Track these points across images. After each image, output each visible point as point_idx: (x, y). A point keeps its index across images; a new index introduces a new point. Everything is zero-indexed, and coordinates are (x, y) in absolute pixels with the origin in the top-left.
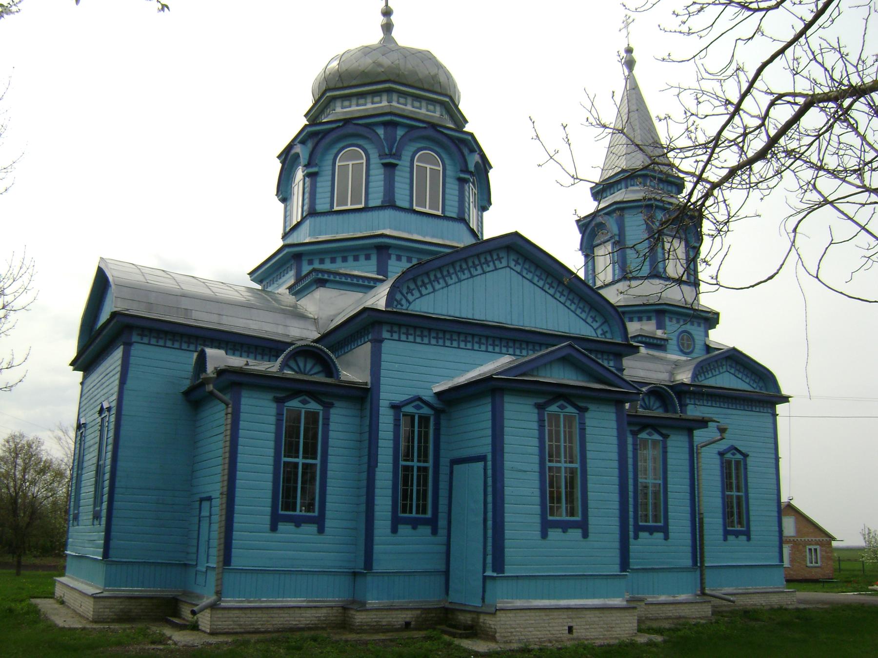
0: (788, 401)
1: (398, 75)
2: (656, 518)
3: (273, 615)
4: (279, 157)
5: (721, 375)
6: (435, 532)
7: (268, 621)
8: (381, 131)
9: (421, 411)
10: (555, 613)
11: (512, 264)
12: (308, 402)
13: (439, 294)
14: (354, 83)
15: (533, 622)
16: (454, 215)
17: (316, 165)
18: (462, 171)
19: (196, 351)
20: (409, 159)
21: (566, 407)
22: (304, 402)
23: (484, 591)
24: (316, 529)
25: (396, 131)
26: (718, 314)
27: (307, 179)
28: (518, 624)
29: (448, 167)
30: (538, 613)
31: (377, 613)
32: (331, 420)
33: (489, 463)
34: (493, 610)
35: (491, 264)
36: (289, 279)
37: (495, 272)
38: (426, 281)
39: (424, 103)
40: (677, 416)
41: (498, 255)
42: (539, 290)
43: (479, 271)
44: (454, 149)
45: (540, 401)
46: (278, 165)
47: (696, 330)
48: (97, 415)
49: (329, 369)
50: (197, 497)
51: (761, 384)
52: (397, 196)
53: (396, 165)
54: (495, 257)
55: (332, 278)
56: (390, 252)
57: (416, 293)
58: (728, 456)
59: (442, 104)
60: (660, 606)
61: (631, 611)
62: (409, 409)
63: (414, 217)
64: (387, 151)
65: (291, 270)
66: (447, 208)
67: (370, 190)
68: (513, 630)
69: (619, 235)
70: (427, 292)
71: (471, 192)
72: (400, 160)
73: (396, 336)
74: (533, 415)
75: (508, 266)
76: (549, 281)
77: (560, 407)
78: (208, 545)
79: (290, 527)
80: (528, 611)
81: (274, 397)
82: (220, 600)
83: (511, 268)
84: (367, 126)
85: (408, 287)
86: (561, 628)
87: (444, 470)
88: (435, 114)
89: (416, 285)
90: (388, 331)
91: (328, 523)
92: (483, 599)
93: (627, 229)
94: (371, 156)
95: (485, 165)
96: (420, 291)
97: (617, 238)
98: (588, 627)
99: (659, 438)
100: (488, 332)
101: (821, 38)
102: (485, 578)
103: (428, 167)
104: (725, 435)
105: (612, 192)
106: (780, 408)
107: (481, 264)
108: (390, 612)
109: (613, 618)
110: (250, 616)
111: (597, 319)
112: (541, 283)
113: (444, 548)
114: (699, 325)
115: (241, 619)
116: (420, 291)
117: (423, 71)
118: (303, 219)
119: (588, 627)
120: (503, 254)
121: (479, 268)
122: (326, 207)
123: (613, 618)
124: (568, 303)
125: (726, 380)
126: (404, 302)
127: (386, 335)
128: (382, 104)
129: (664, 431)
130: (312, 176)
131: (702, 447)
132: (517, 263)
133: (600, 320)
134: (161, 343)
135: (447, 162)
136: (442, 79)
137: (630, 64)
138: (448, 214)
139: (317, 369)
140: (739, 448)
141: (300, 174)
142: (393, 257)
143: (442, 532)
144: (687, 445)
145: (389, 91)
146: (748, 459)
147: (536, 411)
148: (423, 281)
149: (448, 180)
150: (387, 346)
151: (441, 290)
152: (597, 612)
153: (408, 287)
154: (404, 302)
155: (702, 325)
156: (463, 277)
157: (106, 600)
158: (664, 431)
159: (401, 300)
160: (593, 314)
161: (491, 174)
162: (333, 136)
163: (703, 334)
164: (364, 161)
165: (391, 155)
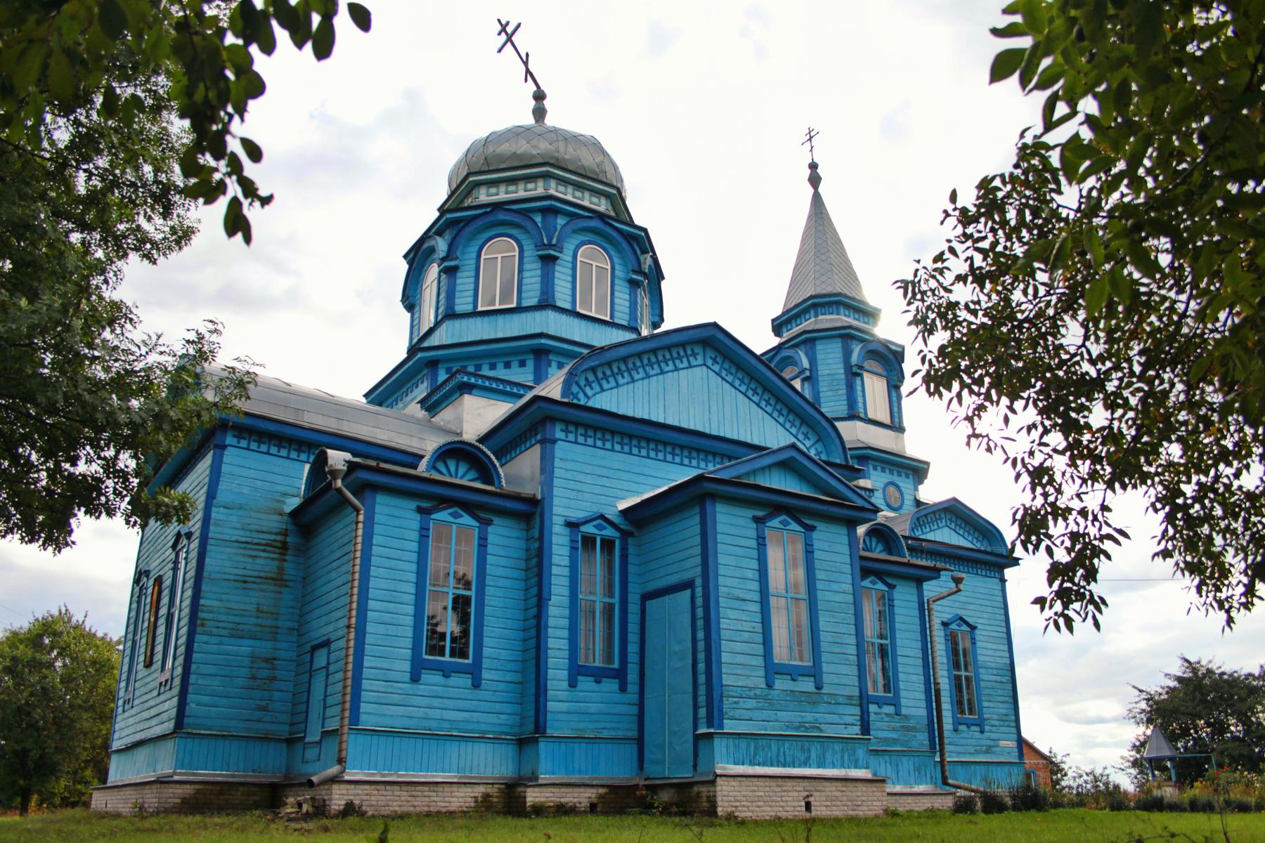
0: (1018, 564)
1: (557, 159)
2: (887, 688)
3: (414, 793)
4: (405, 257)
5: (940, 530)
6: (623, 688)
7: (408, 801)
8: (538, 219)
9: (604, 532)
10: (789, 784)
11: (709, 362)
12: (459, 516)
13: (623, 390)
14: (503, 166)
15: (762, 794)
16: (625, 323)
17: (456, 258)
18: (634, 272)
19: (307, 462)
20: (571, 253)
21: (790, 524)
22: (456, 516)
23: (696, 755)
24: (470, 682)
25: (375, 499)
26: (928, 464)
27: (444, 276)
28: (744, 796)
29: (617, 267)
30: (768, 782)
31: (553, 790)
32: (490, 540)
33: (699, 591)
34: (711, 778)
35: (685, 360)
36: (422, 390)
37: (690, 370)
38: (608, 373)
39: (587, 194)
40: (905, 560)
41: (692, 350)
42: (741, 396)
43: (671, 367)
44: (624, 245)
45: (760, 513)
46: (404, 267)
47: (905, 484)
48: (170, 550)
49: (487, 474)
50: (308, 647)
51: (985, 543)
52: (557, 295)
53: (556, 258)
54: (689, 352)
55: (480, 382)
56: (551, 357)
57: (596, 387)
58: (953, 626)
59: (607, 196)
60: (897, 797)
61: (879, 785)
62: (589, 529)
63: (576, 321)
64: (546, 242)
65: (422, 382)
66: (616, 314)
67: (524, 288)
68: (738, 804)
69: (810, 370)
70: (609, 386)
71: (644, 300)
72: (561, 252)
73: (571, 437)
74: (751, 530)
75: (705, 365)
76: (753, 386)
77: (784, 523)
78: (325, 704)
79: (436, 678)
80: (755, 780)
81: (418, 507)
82: (343, 771)
83: (708, 367)
84: (518, 212)
85: (586, 379)
86: (796, 804)
87: (633, 609)
88: (603, 206)
89: (597, 378)
90: (562, 430)
91: (486, 675)
92: (695, 766)
93: (819, 362)
94: (526, 248)
95: (657, 274)
96: (601, 386)
97: (808, 373)
98: (829, 803)
99: (884, 588)
100: (685, 439)
101: (815, 180)
102: (698, 738)
103: (594, 264)
104: (961, 586)
105: (798, 322)
106: (1008, 573)
107: (673, 359)
108: (571, 790)
109: (859, 794)
110: (384, 793)
111: (809, 436)
112: (743, 388)
113: (635, 710)
114: (907, 476)
115: (372, 798)
116: (601, 386)
117: (588, 160)
118: (438, 324)
119: (829, 803)
120: (698, 349)
121: (670, 363)
122: (469, 308)
123: (859, 794)
124: (775, 414)
125: (946, 535)
126: (581, 395)
127: (559, 434)
128: (539, 189)
129: (889, 581)
130: (450, 271)
131: (934, 601)
132: (715, 361)
133: (813, 438)
134: (264, 448)
135: (616, 260)
136: (608, 168)
137: (815, 180)
138: (616, 321)
139: (472, 474)
140: (966, 618)
141: (433, 271)
142: (554, 364)
143: (633, 688)
144: (915, 598)
145: (546, 176)
146: (977, 632)
147: (754, 526)
148: (604, 373)
149: (617, 281)
150: (561, 449)
151: (626, 387)
152: (838, 784)
153: (586, 379)
154: (581, 395)
155: (911, 477)
156: (652, 372)
157: (178, 786)
158: (889, 581)
159: (578, 393)
160: (804, 429)
161: (663, 284)
162: (479, 223)
163: (912, 487)
164: (517, 254)
165: (550, 246)
